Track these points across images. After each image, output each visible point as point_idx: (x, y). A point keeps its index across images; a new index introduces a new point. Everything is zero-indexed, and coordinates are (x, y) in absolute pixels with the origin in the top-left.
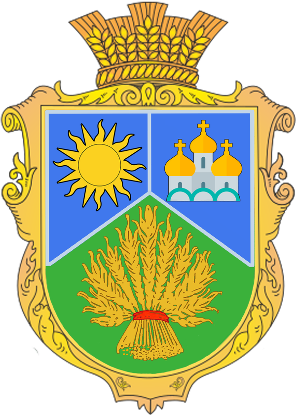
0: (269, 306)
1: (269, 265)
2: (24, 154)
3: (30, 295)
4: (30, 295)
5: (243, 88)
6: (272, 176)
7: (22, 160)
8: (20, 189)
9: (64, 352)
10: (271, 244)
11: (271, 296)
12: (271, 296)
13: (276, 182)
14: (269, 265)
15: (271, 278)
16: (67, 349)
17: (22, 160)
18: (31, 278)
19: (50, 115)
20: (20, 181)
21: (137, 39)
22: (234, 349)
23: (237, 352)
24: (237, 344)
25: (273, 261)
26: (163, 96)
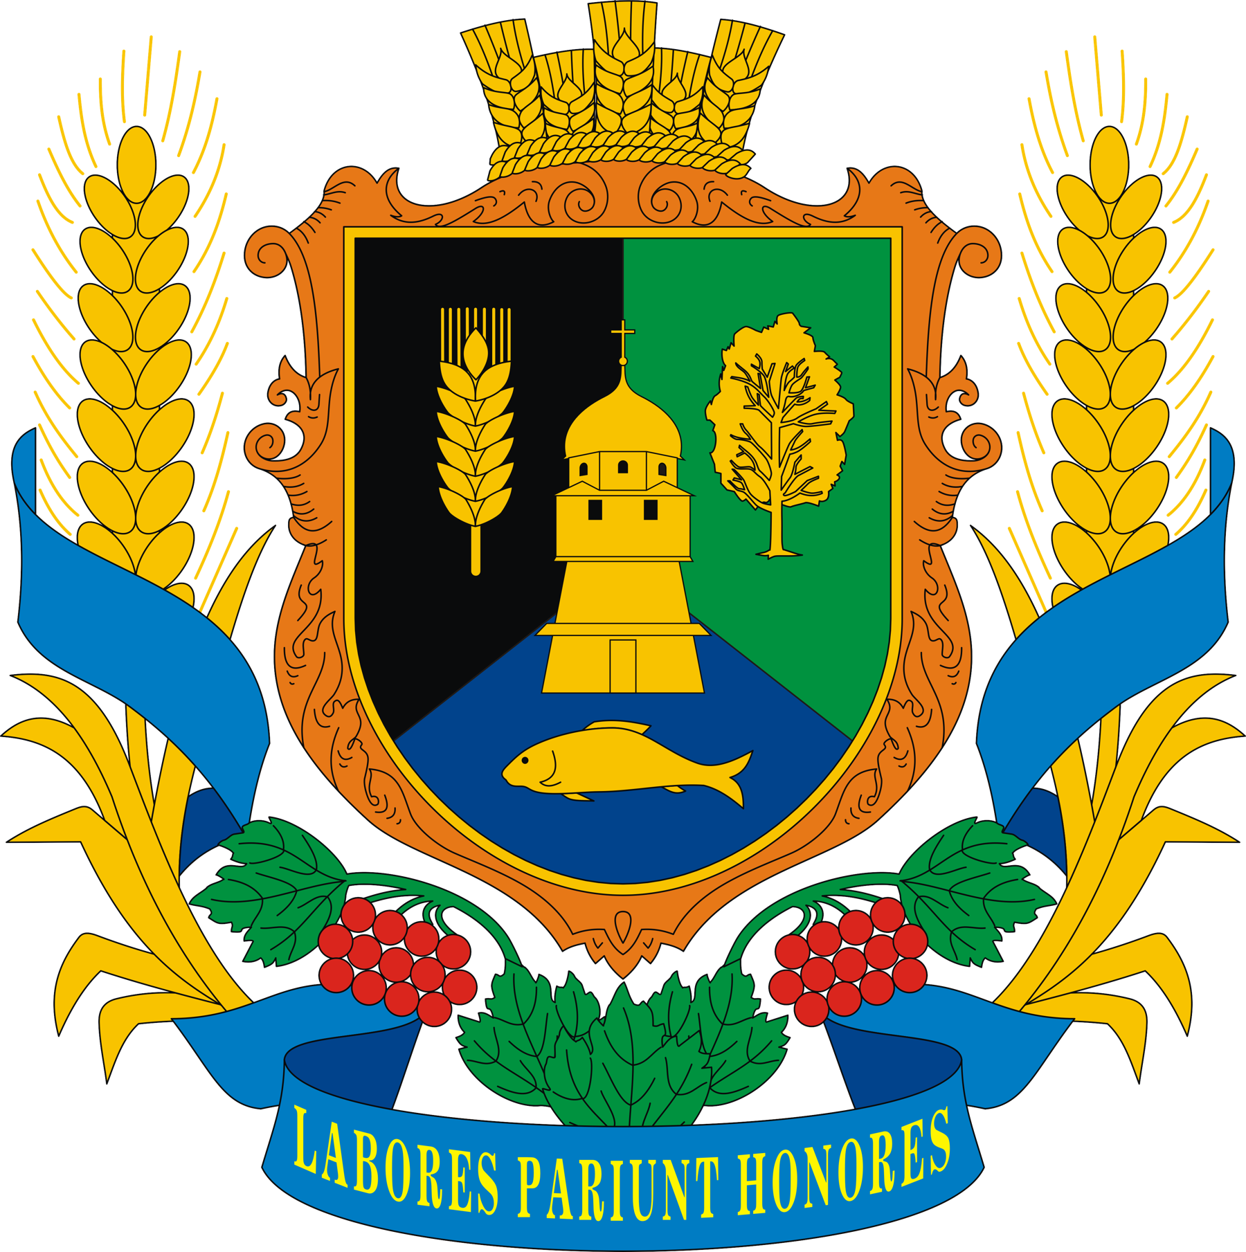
0: (929, 702)
1: (933, 602)
2: (302, 352)
3: (306, 678)
4: (306, 678)
5: (869, 176)
6: (942, 401)
7: (300, 368)
8: (294, 441)
9: (396, 819)
10: (938, 553)
11: (940, 678)
12: (940, 678)
13: (954, 417)
14: (933, 602)
15: (936, 633)
16: (402, 813)
17: (300, 368)
18: (311, 633)
19: (356, 239)
20: (292, 417)
21: (921, 971)
22: (844, 813)
23: (850, 819)
24: (850, 800)
25: (942, 589)
26: (660, 200)
